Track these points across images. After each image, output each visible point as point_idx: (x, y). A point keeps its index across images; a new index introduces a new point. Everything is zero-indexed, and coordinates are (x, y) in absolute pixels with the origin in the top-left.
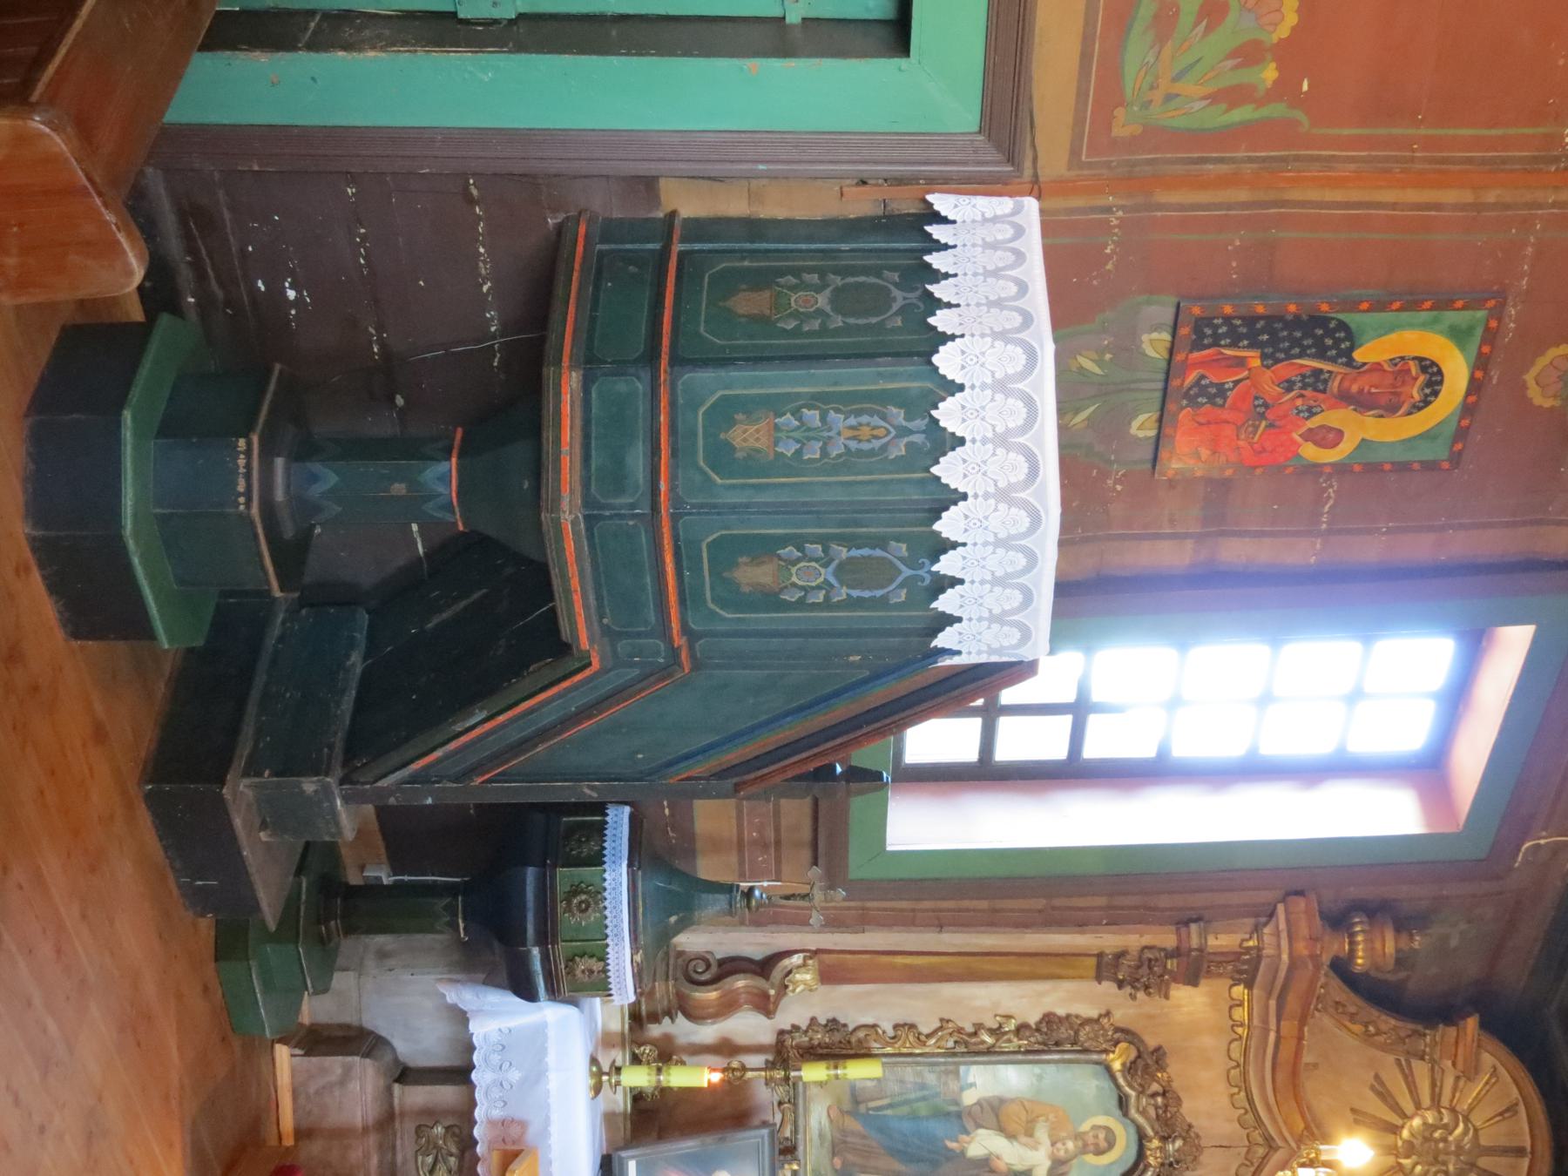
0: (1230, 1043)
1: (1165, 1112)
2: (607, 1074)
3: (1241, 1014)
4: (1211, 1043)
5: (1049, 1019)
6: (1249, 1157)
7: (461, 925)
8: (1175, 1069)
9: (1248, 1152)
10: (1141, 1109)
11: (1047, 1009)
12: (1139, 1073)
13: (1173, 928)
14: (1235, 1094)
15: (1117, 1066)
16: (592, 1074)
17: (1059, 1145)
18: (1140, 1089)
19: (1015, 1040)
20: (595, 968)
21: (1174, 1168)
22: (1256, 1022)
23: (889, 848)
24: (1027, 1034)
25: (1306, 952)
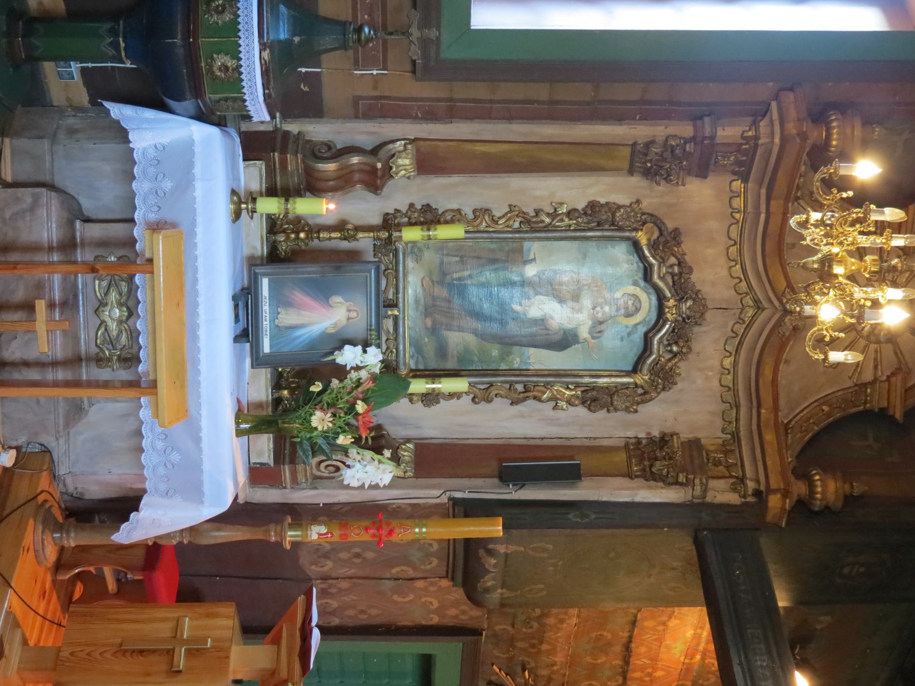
0: (730, 226)
1: (680, 279)
2: (246, 203)
3: (738, 203)
4: (715, 226)
5: (593, 206)
6: (742, 316)
7: (122, 44)
8: (687, 246)
9: (741, 313)
10: (662, 275)
11: (592, 199)
12: (661, 248)
13: (691, 123)
14: (732, 266)
15: (644, 242)
16: (232, 202)
17: (598, 309)
18: (661, 261)
19: (566, 220)
20: (229, 64)
21: (686, 323)
22: (750, 209)
23: (472, 28)
24: (576, 215)
25: (794, 132)
